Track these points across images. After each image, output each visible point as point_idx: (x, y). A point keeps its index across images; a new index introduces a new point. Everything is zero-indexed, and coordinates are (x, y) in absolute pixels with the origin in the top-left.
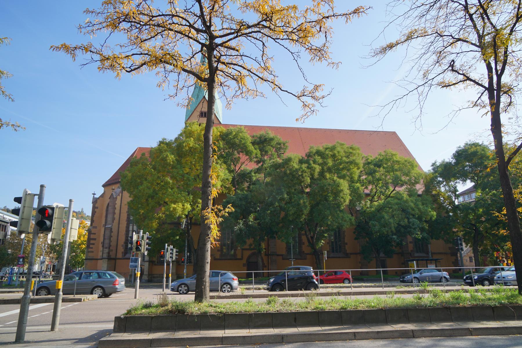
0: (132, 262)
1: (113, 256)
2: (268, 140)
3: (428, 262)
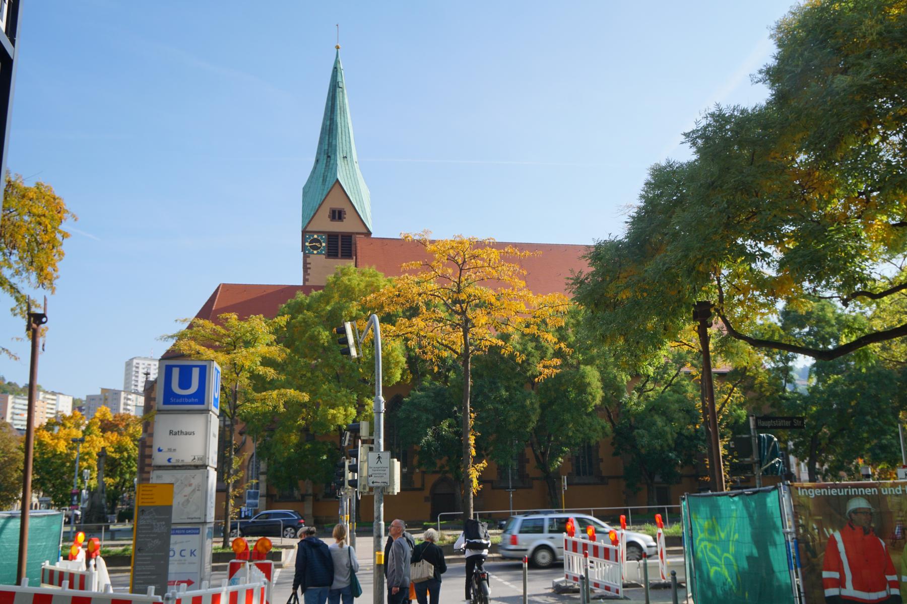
0: (249, 498)
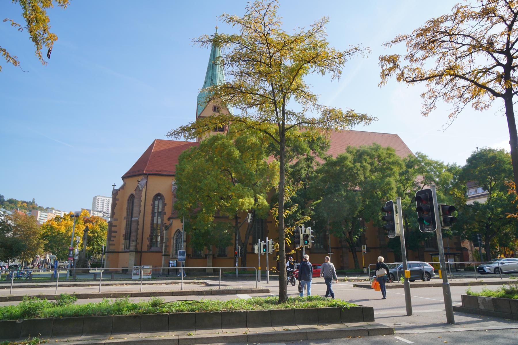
0: (180, 255)
1: (139, 250)
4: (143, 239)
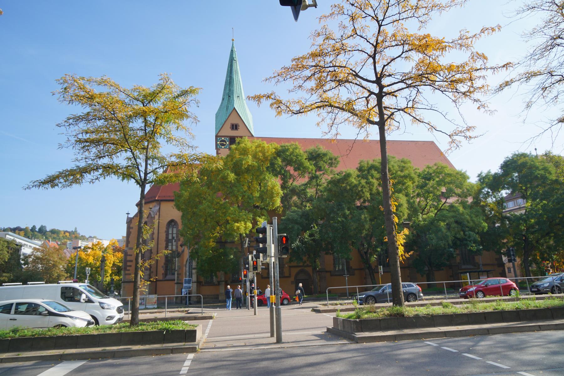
0: (185, 283)
2: (321, 155)
3: (480, 273)
4: (158, 267)
